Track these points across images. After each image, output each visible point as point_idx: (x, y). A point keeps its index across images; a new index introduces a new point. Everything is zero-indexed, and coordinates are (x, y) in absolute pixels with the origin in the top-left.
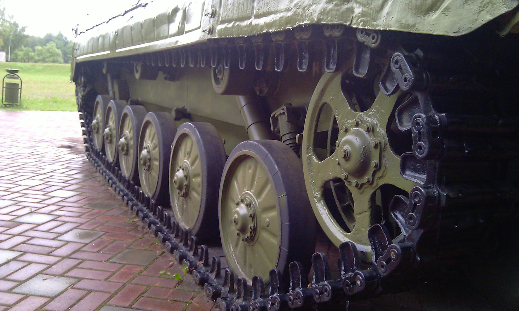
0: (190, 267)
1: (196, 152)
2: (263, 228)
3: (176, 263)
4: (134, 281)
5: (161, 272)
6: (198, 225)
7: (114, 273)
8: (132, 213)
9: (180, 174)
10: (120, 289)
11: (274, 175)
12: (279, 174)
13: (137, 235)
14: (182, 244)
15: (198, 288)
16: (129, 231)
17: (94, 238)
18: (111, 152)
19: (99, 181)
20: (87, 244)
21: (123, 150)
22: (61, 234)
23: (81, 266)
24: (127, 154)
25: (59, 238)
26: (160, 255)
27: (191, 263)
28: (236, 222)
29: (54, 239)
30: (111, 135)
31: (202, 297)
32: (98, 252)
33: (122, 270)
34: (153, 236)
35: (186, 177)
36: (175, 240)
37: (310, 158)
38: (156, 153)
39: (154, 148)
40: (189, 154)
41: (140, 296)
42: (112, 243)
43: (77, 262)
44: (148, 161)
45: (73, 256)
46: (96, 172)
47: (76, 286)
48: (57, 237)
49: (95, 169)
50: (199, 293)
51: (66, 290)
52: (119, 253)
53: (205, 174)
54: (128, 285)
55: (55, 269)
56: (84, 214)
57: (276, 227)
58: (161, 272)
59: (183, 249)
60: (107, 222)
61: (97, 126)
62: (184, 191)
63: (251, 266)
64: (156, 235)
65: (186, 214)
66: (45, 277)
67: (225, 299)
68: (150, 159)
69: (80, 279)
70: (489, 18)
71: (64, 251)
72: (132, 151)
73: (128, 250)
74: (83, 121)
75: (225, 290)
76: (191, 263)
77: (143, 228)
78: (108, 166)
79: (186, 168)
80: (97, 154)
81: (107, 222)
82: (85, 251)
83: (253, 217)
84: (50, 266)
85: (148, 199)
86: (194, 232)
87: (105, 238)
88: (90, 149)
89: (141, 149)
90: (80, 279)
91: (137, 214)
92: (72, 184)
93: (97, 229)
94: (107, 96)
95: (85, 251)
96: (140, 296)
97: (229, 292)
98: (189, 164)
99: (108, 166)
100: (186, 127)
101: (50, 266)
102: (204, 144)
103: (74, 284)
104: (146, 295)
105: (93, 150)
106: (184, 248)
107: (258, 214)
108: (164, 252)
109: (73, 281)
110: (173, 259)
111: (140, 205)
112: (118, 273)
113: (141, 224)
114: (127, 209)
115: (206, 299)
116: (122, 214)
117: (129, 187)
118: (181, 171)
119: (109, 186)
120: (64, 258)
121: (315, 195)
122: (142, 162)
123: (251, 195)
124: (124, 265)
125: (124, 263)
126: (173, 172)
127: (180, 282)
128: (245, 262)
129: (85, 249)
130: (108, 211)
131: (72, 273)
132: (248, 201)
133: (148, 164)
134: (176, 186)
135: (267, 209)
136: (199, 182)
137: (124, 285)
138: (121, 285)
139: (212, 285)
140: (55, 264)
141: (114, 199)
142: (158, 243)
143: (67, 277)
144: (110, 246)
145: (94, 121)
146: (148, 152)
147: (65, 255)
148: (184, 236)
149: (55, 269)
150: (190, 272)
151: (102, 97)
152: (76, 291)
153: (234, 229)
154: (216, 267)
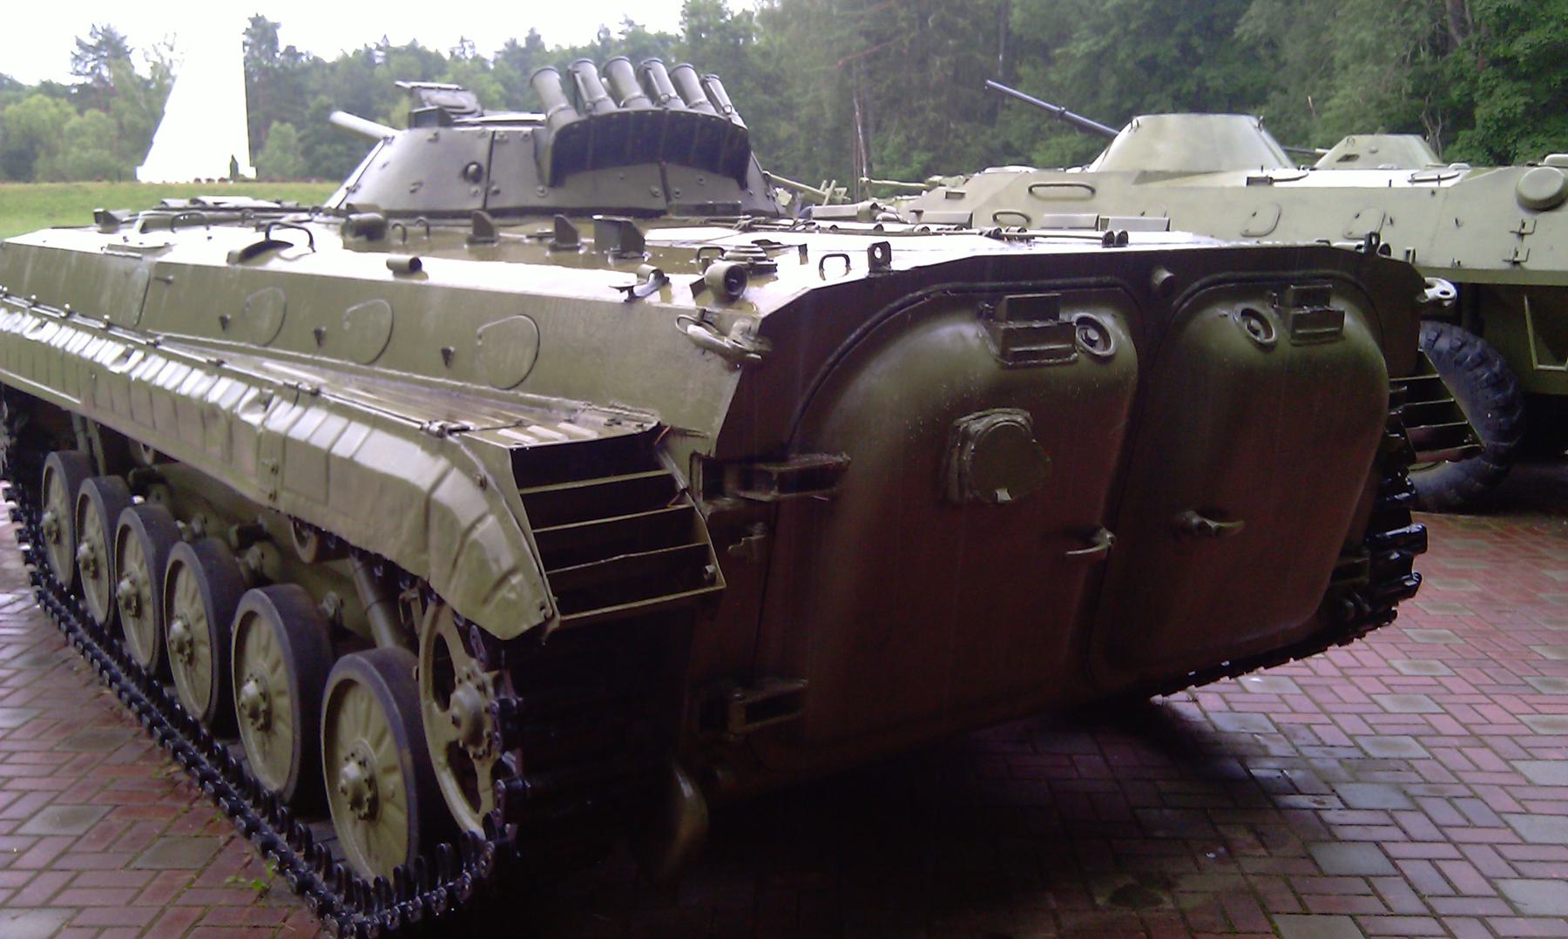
0: (281, 864)
1: (276, 650)
2: (388, 800)
3: (257, 856)
4: (179, 901)
5: (228, 880)
6: (293, 785)
7: (142, 890)
8: (163, 754)
9: (250, 689)
10: (158, 917)
11: (393, 720)
12: (400, 719)
13: (177, 804)
14: (266, 819)
15: (295, 901)
16: (161, 798)
17: (93, 821)
18: (100, 597)
19: (78, 672)
20: (79, 838)
21: (128, 605)
22: (22, 822)
23: (75, 883)
24: (139, 613)
25: (22, 831)
26: (227, 844)
27: (282, 855)
28: (344, 791)
29: (10, 834)
30: (95, 561)
31: (302, 915)
32: (106, 850)
33: (157, 882)
34: (210, 803)
35: (265, 696)
36: (253, 813)
37: (429, 708)
38: (202, 629)
39: (199, 620)
40: (266, 649)
41: (194, 926)
42: (130, 828)
43: (67, 876)
44: (187, 647)
45: (57, 865)
46: (67, 644)
47: (75, 922)
48: (16, 829)
49: (62, 636)
50: (299, 908)
51: (59, 931)
52: (147, 848)
53: (295, 691)
54: (170, 911)
55: (30, 896)
56: (61, 766)
57: (401, 798)
58: (228, 880)
59: (269, 830)
60: (113, 781)
61: (54, 528)
62: (261, 721)
63: (377, 858)
64: (217, 803)
65: (269, 762)
66: (13, 913)
67: (337, 915)
68: (191, 643)
69: (80, 909)
70: (526, 627)
71: (36, 858)
72: (149, 610)
73: (162, 840)
74: (27, 547)
75: (337, 899)
76: (282, 855)
77: (190, 786)
78: (95, 630)
79: (262, 677)
80: (64, 597)
81: (113, 781)
82: (78, 853)
83: (371, 782)
84: (18, 891)
85: (196, 724)
86: (287, 797)
87: (113, 819)
88: (41, 578)
89: (171, 618)
90: (80, 909)
91: (175, 757)
92: (16, 690)
93: (94, 800)
94: (73, 453)
95: (78, 853)
96: (194, 926)
97: (345, 902)
98: (266, 669)
99: (95, 630)
100: (254, 600)
101: (18, 891)
102: (291, 637)
103: (71, 920)
104: (201, 923)
105: (51, 584)
106: (270, 827)
107: (378, 777)
108: (233, 838)
109: (68, 913)
110: (251, 849)
111: (180, 737)
112: (149, 889)
113: (183, 777)
114: (150, 743)
115: (310, 917)
116: (141, 758)
117: (154, 693)
118: (252, 683)
119: (102, 684)
120: (40, 871)
121: (438, 758)
122: (175, 647)
123: (365, 746)
124: (159, 871)
125: (158, 867)
126: (240, 685)
127: (264, 893)
128: (369, 849)
129: (78, 847)
130: (110, 754)
131: (62, 899)
132: (360, 757)
133: (187, 651)
134: (246, 712)
135: (389, 770)
136: (285, 705)
137: (163, 911)
138: (157, 910)
139: (316, 894)
140: (24, 886)
141: (119, 718)
142: (220, 818)
143: (56, 907)
144: (127, 836)
145: (47, 517)
146: (187, 627)
147: (41, 864)
148: (268, 803)
149: (30, 896)
150: (281, 872)
151: (63, 459)
152: (79, 931)
153: (346, 801)
154: (323, 860)
